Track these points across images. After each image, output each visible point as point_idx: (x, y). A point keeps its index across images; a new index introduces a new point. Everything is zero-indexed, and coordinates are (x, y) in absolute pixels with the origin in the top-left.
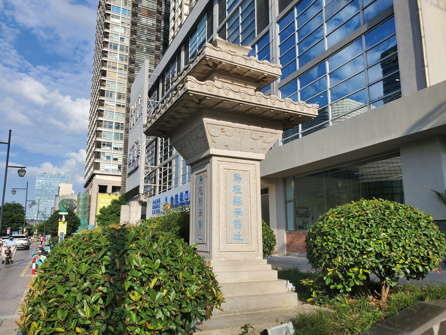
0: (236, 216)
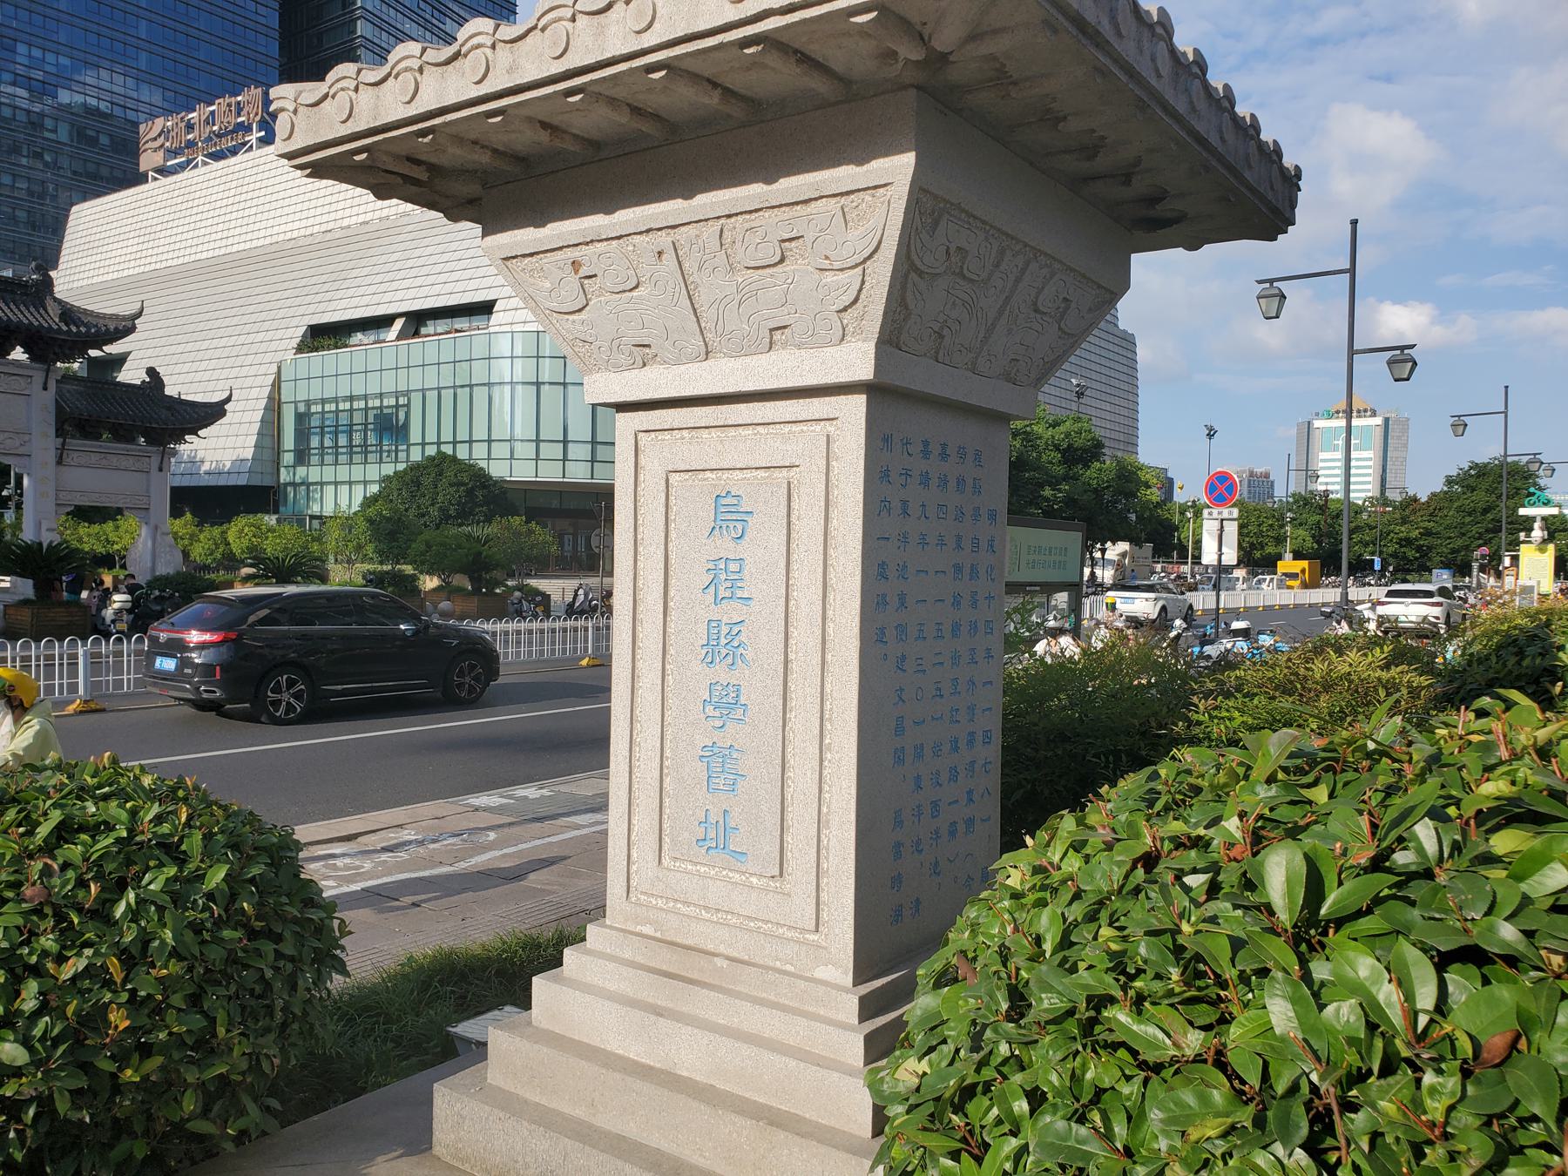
0: (718, 723)
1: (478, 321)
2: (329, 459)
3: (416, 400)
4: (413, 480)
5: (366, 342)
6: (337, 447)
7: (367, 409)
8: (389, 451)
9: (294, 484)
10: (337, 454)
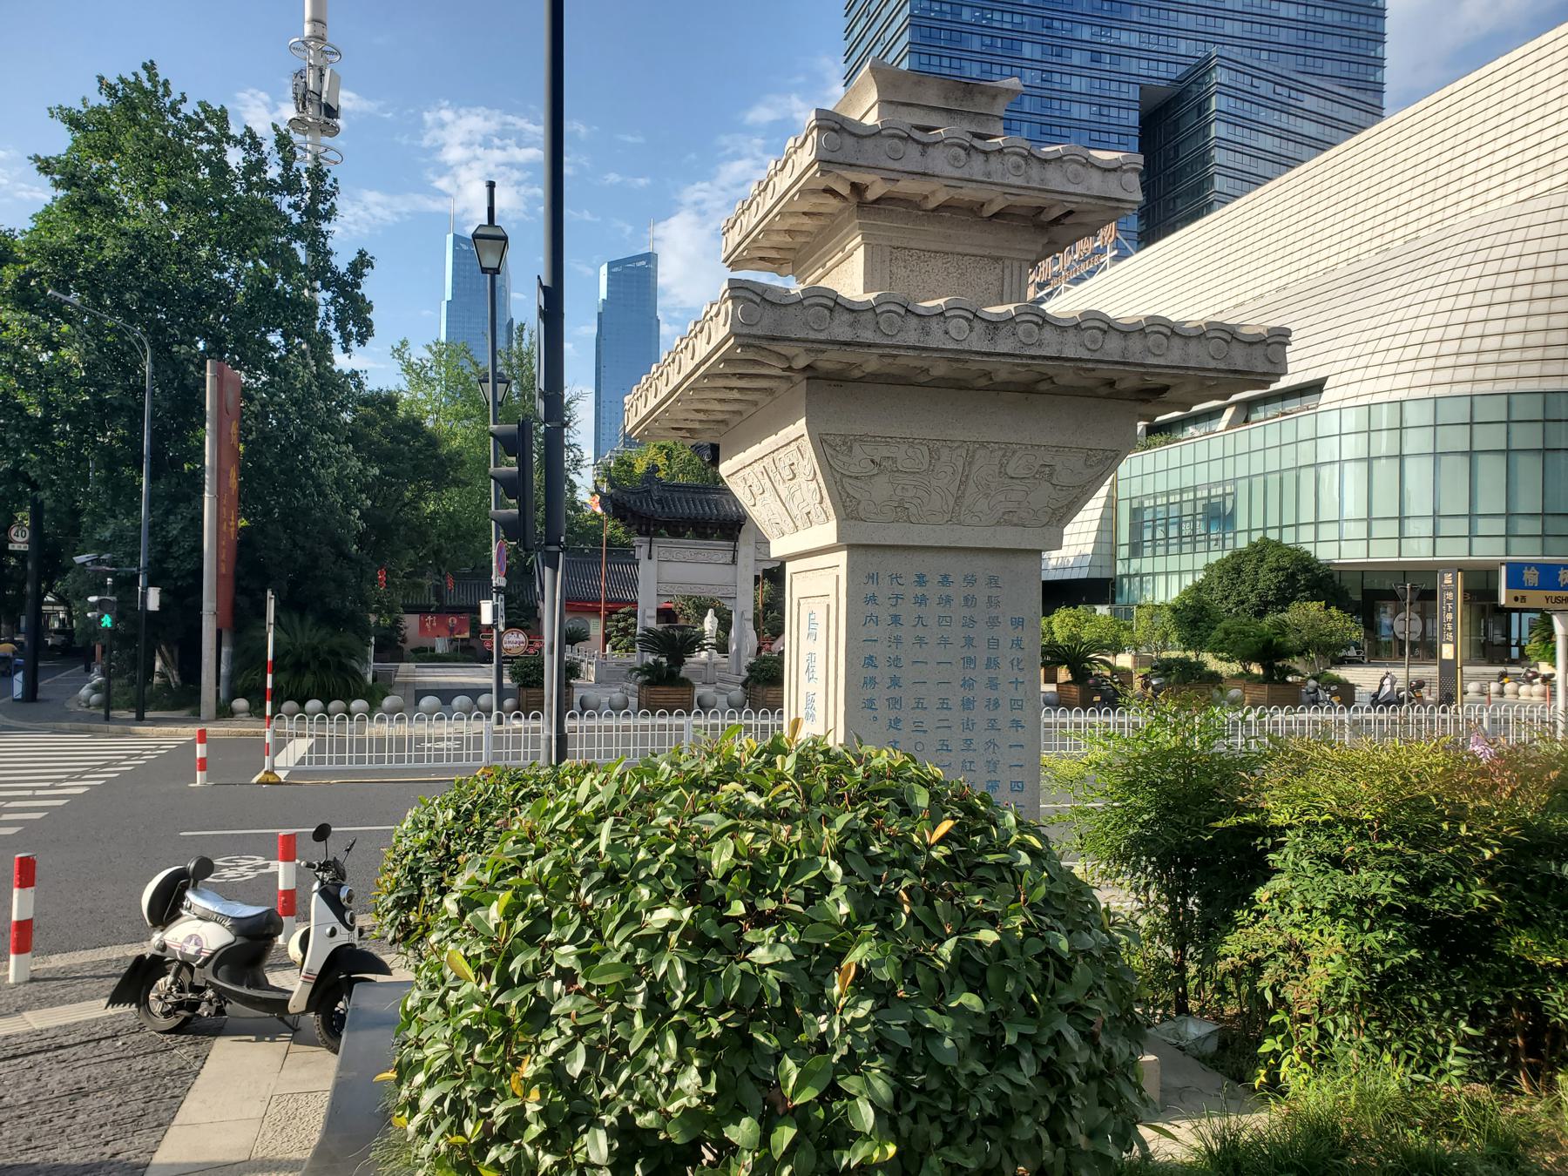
1: (1308, 400)
2: (1161, 550)
3: (1243, 485)
4: (1234, 568)
5: (1197, 434)
6: (1167, 538)
7: (1195, 500)
8: (1217, 540)
9: (1128, 576)
10: (1167, 545)
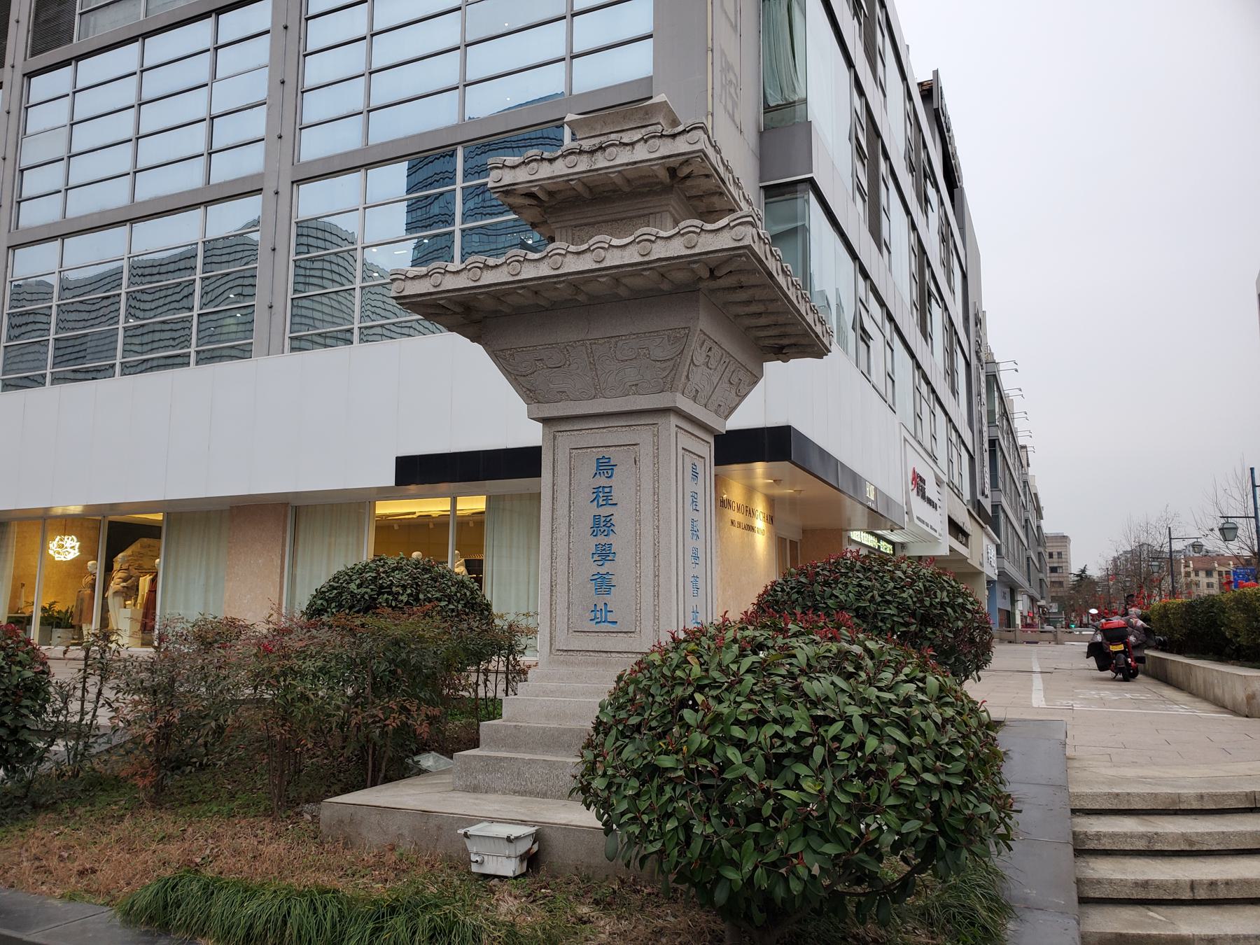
0: (600, 563)
